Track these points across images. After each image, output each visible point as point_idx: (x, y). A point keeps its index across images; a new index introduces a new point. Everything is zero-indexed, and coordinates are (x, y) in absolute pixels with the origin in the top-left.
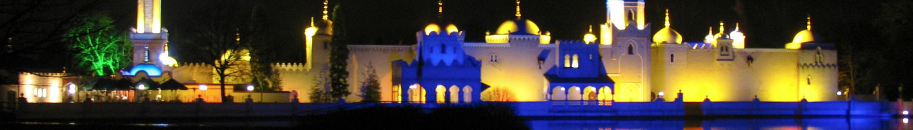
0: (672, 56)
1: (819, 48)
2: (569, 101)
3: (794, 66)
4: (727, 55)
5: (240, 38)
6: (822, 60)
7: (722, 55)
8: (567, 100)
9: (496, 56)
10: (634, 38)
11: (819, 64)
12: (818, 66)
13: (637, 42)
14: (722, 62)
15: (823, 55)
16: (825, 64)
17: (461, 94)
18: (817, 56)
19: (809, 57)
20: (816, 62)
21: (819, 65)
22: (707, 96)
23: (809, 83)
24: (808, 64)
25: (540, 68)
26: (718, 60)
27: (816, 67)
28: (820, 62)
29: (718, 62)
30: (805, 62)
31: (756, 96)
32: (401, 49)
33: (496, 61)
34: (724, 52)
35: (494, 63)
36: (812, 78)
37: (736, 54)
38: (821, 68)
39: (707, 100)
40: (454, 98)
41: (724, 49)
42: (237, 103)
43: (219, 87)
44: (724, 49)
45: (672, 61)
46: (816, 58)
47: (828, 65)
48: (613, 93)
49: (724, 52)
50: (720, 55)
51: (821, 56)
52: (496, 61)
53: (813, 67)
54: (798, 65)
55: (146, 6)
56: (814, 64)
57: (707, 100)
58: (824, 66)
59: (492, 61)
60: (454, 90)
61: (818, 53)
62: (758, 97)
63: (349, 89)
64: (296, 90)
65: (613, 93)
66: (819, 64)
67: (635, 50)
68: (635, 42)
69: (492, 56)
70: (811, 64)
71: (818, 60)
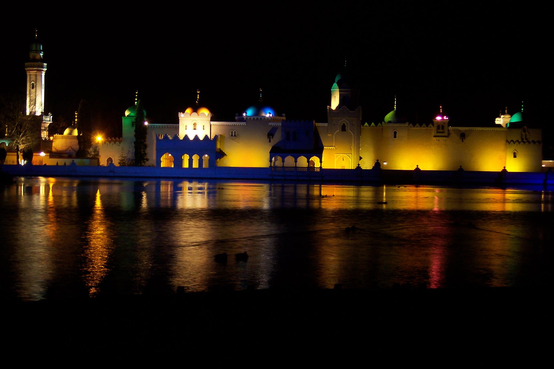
0: (395, 133)
1: (525, 127)
2: (285, 167)
3: (504, 142)
4: (444, 132)
5: (75, 121)
6: (528, 137)
7: (438, 132)
8: (296, 167)
9: (235, 132)
10: (345, 118)
11: (525, 140)
12: (524, 142)
13: (348, 121)
14: (437, 138)
15: (528, 132)
16: (530, 141)
17: (201, 162)
18: (524, 134)
19: (516, 135)
20: (522, 139)
21: (524, 141)
22: (417, 166)
23: (515, 157)
24: (515, 140)
25: (270, 142)
26: (435, 136)
27: (522, 143)
28: (526, 139)
29: (434, 138)
30: (512, 139)
31: (461, 167)
32: (169, 127)
33: (235, 136)
34: (441, 130)
35: (234, 137)
36: (517, 151)
37: (451, 132)
38: (527, 143)
39: (417, 169)
40: (195, 165)
41: (441, 128)
42: (36, 166)
43: (16, 156)
44: (441, 128)
45: (395, 137)
46: (522, 135)
47: (534, 142)
48: (321, 162)
49: (441, 130)
50: (436, 132)
51: (527, 133)
52: (235, 136)
53: (519, 143)
54: (507, 141)
55: (31, 96)
56: (520, 140)
57: (417, 169)
58: (529, 142)
59: (232, 136)
60: (196, 158)
61: (525, 131)
62: (462, 167)
63: (148, 156)
64: (111, 157)
65: (321, 162)
66: (525, 140)
67: (348, 128)
68: (348, 121)
69: (232, 132)
70: (517, 141)
71: (524, 137)
